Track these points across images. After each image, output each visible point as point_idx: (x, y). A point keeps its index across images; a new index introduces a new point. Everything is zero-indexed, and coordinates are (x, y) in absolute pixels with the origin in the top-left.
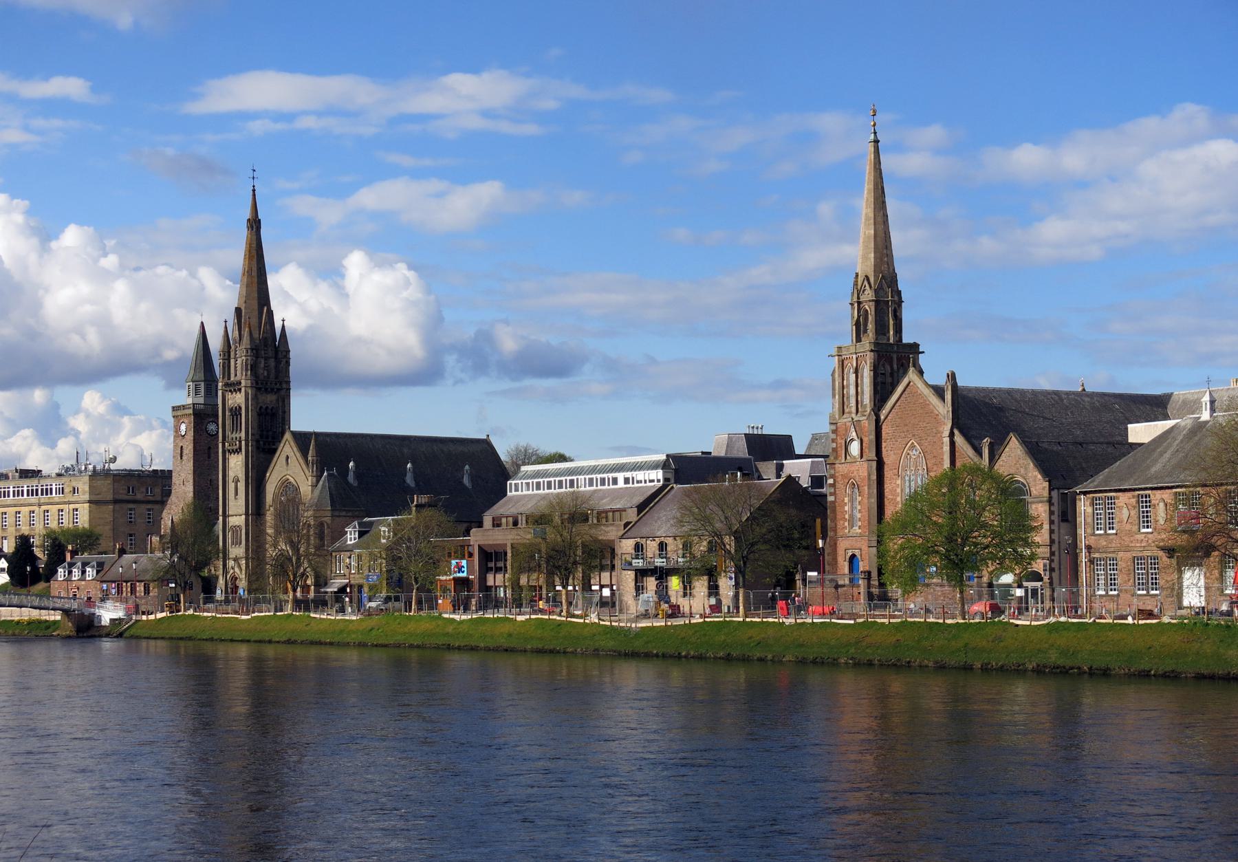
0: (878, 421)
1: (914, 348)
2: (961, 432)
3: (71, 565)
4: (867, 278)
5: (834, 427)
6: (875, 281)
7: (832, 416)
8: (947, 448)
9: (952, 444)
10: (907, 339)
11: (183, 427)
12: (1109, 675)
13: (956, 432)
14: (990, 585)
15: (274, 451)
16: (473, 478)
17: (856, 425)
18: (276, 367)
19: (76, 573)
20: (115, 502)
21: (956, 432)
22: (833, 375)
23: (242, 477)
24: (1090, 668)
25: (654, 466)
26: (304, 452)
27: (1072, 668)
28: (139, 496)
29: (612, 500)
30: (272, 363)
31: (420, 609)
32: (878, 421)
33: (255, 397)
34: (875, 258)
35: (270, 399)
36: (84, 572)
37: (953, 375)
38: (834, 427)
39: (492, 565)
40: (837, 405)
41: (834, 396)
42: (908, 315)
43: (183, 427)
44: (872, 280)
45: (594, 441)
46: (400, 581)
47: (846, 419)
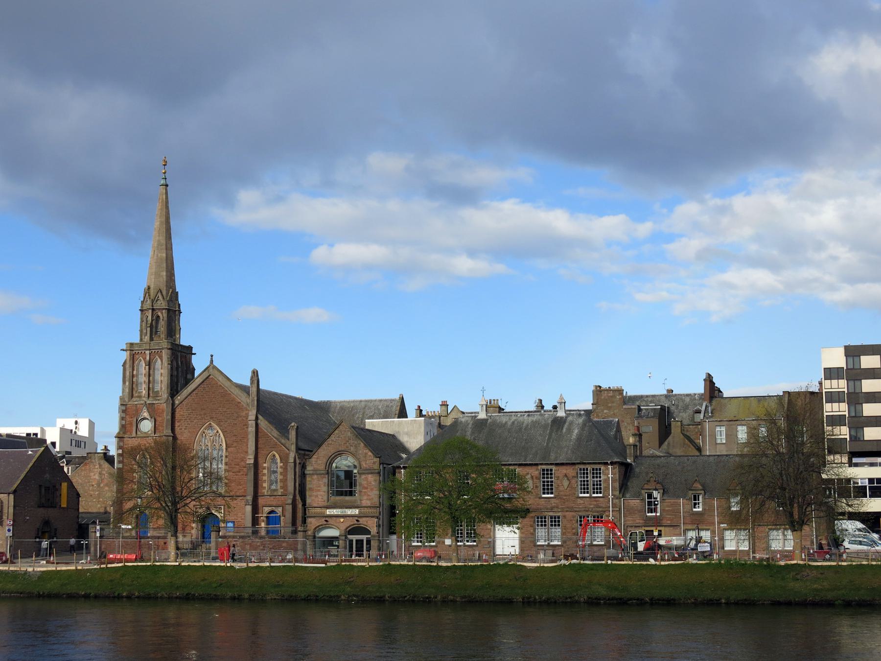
0: (173, 404)
1: (598, 391)
5: (124, 408)
6: (167, 293)
7: (121, 399)
8: (252, 429)
9: (257, 425)
12: (430, 602)
13: (260, 417)
14: (314, 537)
17: (151, 408)
21: (260, 417)
22: (124, 365)
24: (651, 599)
27: (631, 599)
32: (173, 404)
34: (167, 276)
37: (541, 401)
38: (124, 408)
40: (127, 390)
41: (124, 382)
42: (185, 321)
44: (164, 293)
46: (142, 557)
47: (135, 401)
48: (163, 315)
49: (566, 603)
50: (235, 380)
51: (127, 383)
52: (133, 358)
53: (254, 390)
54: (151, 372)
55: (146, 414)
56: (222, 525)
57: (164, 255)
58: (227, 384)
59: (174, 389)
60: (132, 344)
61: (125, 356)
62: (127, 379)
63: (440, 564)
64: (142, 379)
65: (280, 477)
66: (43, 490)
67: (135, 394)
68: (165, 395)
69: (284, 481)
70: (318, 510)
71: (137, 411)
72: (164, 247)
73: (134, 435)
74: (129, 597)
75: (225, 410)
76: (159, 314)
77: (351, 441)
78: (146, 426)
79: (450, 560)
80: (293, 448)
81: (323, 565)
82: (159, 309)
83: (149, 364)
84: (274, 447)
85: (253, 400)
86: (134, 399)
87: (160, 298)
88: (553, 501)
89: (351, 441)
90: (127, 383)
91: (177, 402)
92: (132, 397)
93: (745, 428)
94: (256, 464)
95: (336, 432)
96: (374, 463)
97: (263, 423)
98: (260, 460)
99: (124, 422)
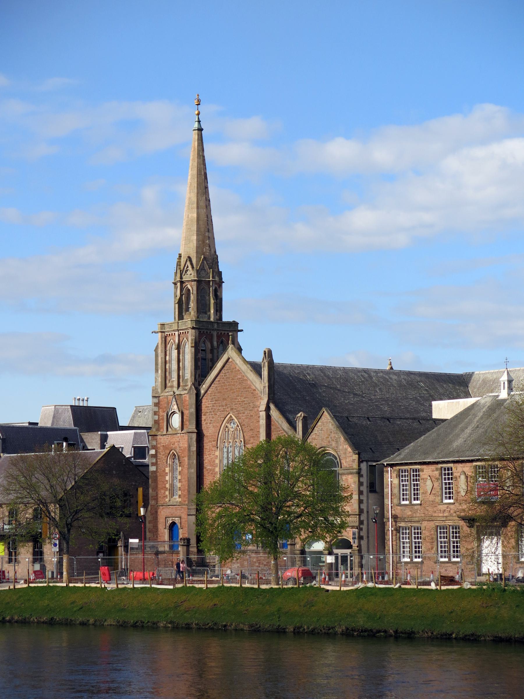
0: (198, 395)
5: (156, 400)
7: (154, 390)
8: (263, 422)
9: (268, 417)
13: (272, 406)
14: (303, 552)
17: (177, 398)
24: (396, 632)
32: (198, 395)
34: (198, 240)
38: (156, 400)
40: (160, 380)
41: (157, 371)
44: (194, 261)
49: (328, 634)
51: (160, 371)
54: (181, 358)
57: (195, 215)
60: (163, 325)
62: (159, 366)
63: (136, 586)
67: (169, 384)
72: (195, 205)
73: (165, 433)
75: (243, 399)
76: (189, 286)
77: (333, 435)
79: (268, 582)
81: (171, 587)
82: (188, 281)
85: (264, 387)
86: (167, 390)
87: (190, 268)
88: (452, 506)
89: (333, 435)
90: (160, 371)
91: (202, 392)
92: (165, 387)
95: (319, 423)
96: (354, 460)
97: (275, 413)
99: (156, 418)
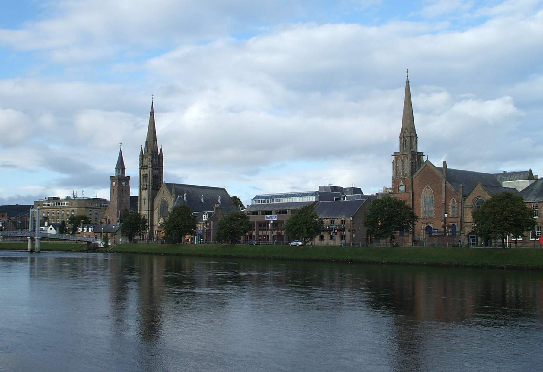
1: (129, 178)
2: (449, 182)
3: (83, 227)
4: (406, 129)
8: (444, 188)
10: (419, 150)
11: (114, 183)
15: (158, 190)
16: (204, 200)
17: (404, 180)
18: (159, 161)
19: (85, 230)
20: (86, 208)
21: (447, 182)
23: (147, 197)
25: (312, 194)
26: (170, 190)
28: (93, 206)
29: (264, 207)
30: (157, 159)
31: (371, 243)
33: (152, 171)
35: (157, 172)
36: (88, 229)
39: (262, 228)
43: (114, 183)
45: (62, 196)
48: (408, 139)
50: (436, 166)
52: (396, 159)
53: (444, 170)
55: (402, 183)
56: (433, 231)
58: (433, 168)
59: (413, 172)
61: (393, 158)
64: (401, 168)
65: (456, 209)
66: (29, 246)
68: (409, 174)
69: (457, 211)
70: (469, 224)
71: (399, 182)
74: (151, 297)
78: (402, 188)
80: (461, 196)
83: (403, 161)
84: (453, 196)
93: (314, 200)
94: (445, 204)
97: (449, 185)
98: (447, 202)
